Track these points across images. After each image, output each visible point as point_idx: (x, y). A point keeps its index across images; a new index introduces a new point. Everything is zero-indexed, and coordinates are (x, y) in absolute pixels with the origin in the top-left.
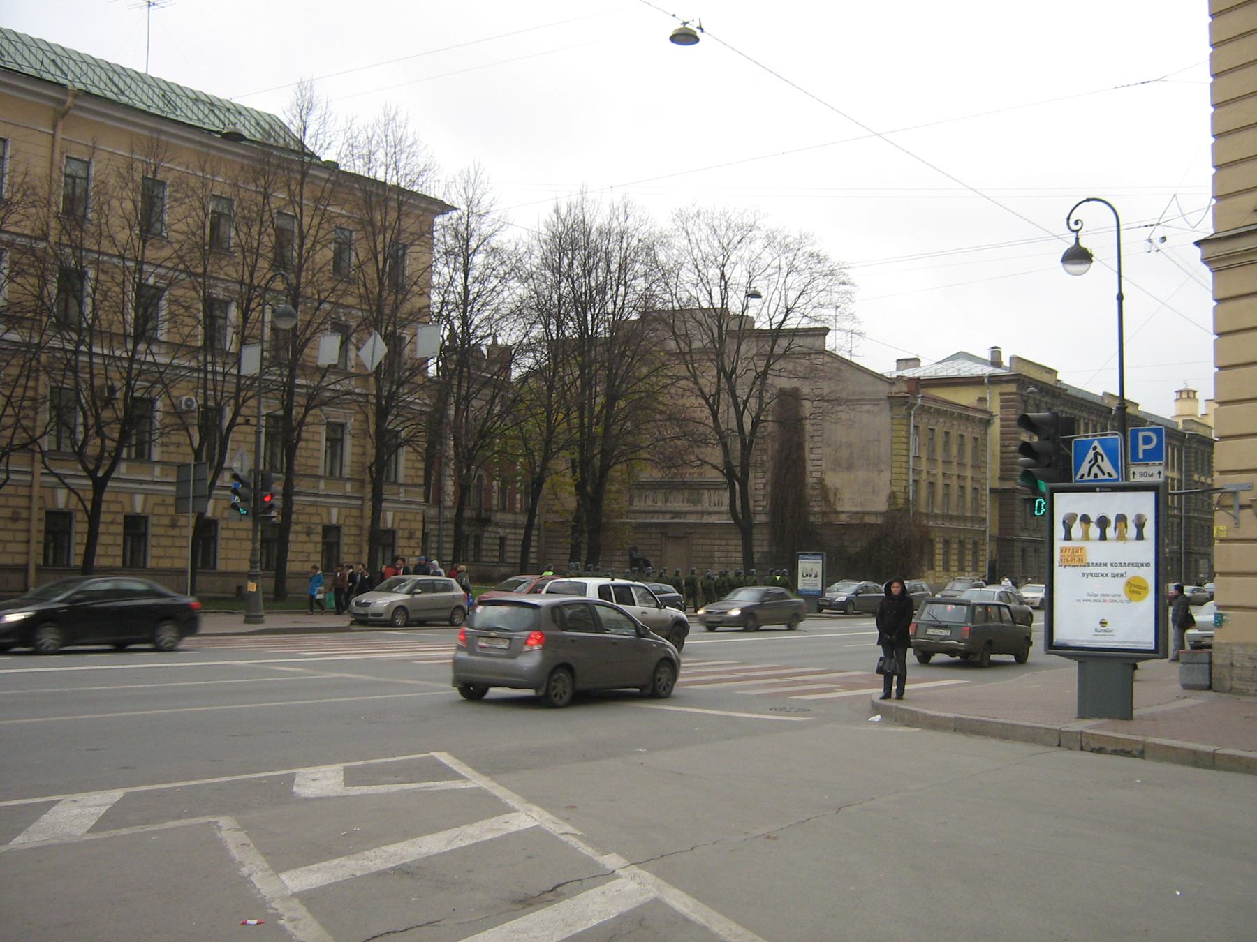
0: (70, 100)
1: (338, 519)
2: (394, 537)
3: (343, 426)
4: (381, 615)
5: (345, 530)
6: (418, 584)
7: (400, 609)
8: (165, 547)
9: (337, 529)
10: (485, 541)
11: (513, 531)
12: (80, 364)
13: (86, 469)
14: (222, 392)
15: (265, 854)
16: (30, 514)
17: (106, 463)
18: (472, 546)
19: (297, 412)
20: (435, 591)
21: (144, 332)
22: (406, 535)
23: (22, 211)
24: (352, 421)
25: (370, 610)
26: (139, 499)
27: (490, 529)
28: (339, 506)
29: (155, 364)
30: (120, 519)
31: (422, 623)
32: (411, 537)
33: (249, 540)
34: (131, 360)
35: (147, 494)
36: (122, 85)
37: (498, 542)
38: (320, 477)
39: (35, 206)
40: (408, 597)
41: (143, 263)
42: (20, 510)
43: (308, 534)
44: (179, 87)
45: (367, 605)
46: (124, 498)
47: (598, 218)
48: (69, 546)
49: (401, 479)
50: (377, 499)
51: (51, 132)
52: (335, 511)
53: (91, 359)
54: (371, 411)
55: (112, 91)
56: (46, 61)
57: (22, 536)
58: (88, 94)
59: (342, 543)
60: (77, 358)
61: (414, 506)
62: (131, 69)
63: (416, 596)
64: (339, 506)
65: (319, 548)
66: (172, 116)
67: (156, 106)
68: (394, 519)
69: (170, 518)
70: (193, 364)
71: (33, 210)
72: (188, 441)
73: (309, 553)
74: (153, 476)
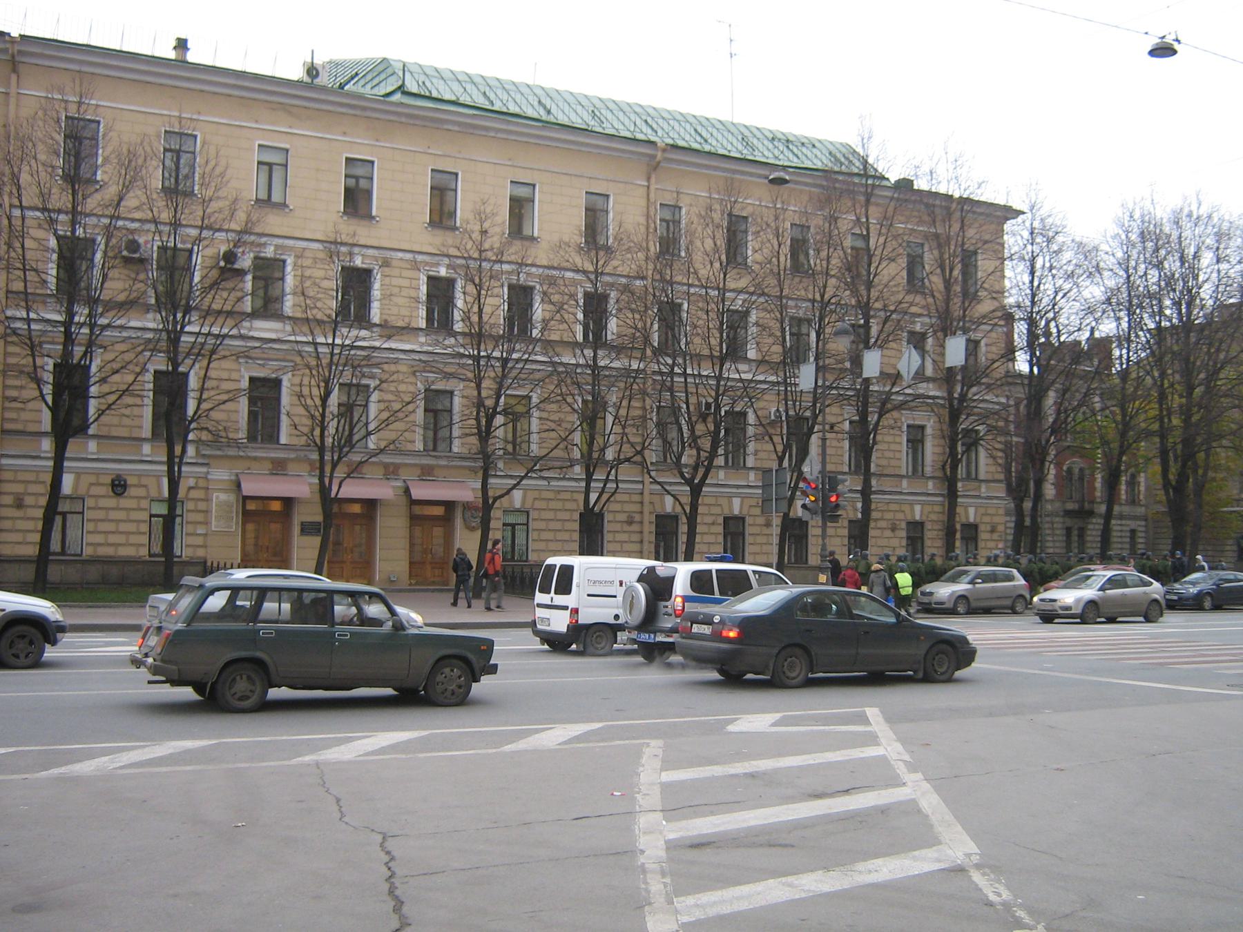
0: (659, 155)
1: (921, 516)
2: (976, 531)
3: (922, 428)
4: (942, 603)
5: (928, 526)
6: (979, 575)
7: (962, 597)
8: (622, 542)
9: (741, 520)
10: (1089, 532)
11: (1119, 522)
12: (33, 333)
13: (682, 476)
14: (800, 401)
15: (919, 811)
16: (642, 518)
17: (701, 471)
18: (1076, 538)
19: (873, 418)
20: (996, 581)
21: (734, 351)
22: (989, 528)
23: (620, 258)
24: (931, 426)
25: (935, 598)
26: (736, 502)
27: (1094, 521)
28: (923, 504)
29: (741, 380)
30: (721, 520)
31: (987, 611)
32: (993, 531)
33: (38, 531)
34: (719, 378)
35: (743, 497)
36: (704, 134)
37: (1128, 534)
38: (902, 477)
39: (630, 252)
40: (969, 586)
41: (725, 290)
42: (634, 515)
43: (893, 529)
44: (746, 126)
45: (931, 594)
46: (906, 508)
47: (1163, 213)
48: (602, 543)
49: (982, 476)
50: (952, 494)
51: (646, 184)
52: (918, 508)
53: (316, 349)
54: (945, 413)
55: (696, 141)
56: (638, 122)
57: (636, 537)
58: (675, 147)
59: (925, 538)
60: (672, 379)
61: (995, 501)
62: (650, 106)
63: (977, 585)
64: (918, 502)
65: (904, 543)
66: (750, 158)
67: (735, 149)
68: (922, 512)
69: (627, 514)
70: (773, 378)
71: (629, 256)
72: (772, 449)
73: (894, 548)
74: (748, 481)
